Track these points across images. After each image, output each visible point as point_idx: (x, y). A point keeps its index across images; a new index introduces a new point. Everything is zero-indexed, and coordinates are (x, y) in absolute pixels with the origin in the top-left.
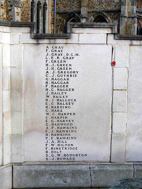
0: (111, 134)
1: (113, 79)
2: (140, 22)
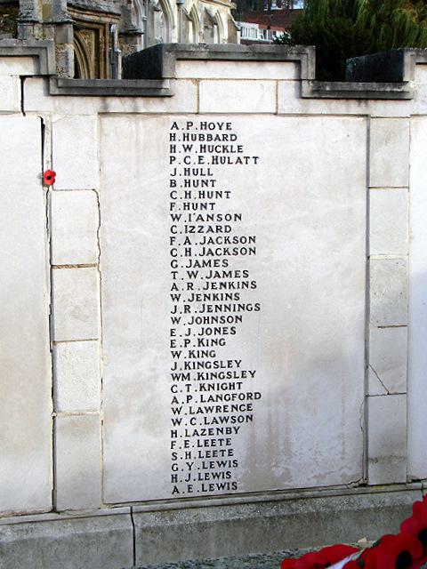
0: (54, 417)
1: (49, 231)
2: (81, 40)
